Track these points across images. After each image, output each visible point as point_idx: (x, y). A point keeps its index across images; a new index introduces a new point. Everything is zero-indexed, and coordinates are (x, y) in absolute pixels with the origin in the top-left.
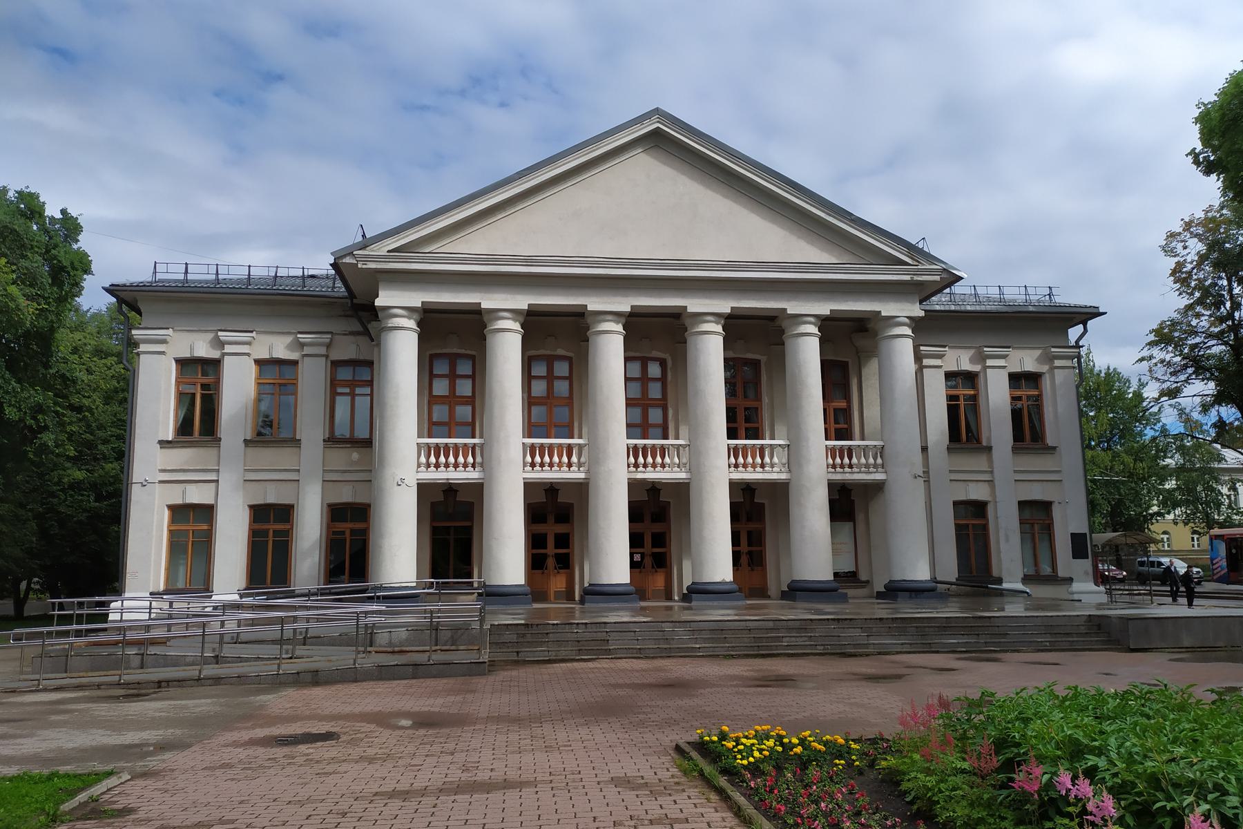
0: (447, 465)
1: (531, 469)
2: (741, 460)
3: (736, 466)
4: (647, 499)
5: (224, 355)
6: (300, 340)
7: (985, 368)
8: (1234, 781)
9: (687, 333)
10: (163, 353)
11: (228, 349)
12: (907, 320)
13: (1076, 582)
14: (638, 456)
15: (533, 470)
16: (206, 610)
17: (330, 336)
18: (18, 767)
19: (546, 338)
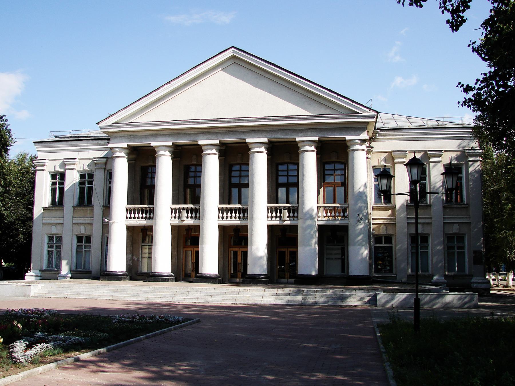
0: (227, 217)
1: (275, 219)
2: (225, 215)
3: (223, 218)
4: (186, 234)
5: (66, 170)
6: (65, 162)
7: (394, 164)
8: (47, 361)
9: (250, 152)
10: (43, 170)
11: (68, 167)
12: (359, 142)
13: (155, 270)
14: (189, 213)
15: (293, 219)
16: (78, 289)
17: (106, 159)
18: (180, 368)
19: (193, 156)
